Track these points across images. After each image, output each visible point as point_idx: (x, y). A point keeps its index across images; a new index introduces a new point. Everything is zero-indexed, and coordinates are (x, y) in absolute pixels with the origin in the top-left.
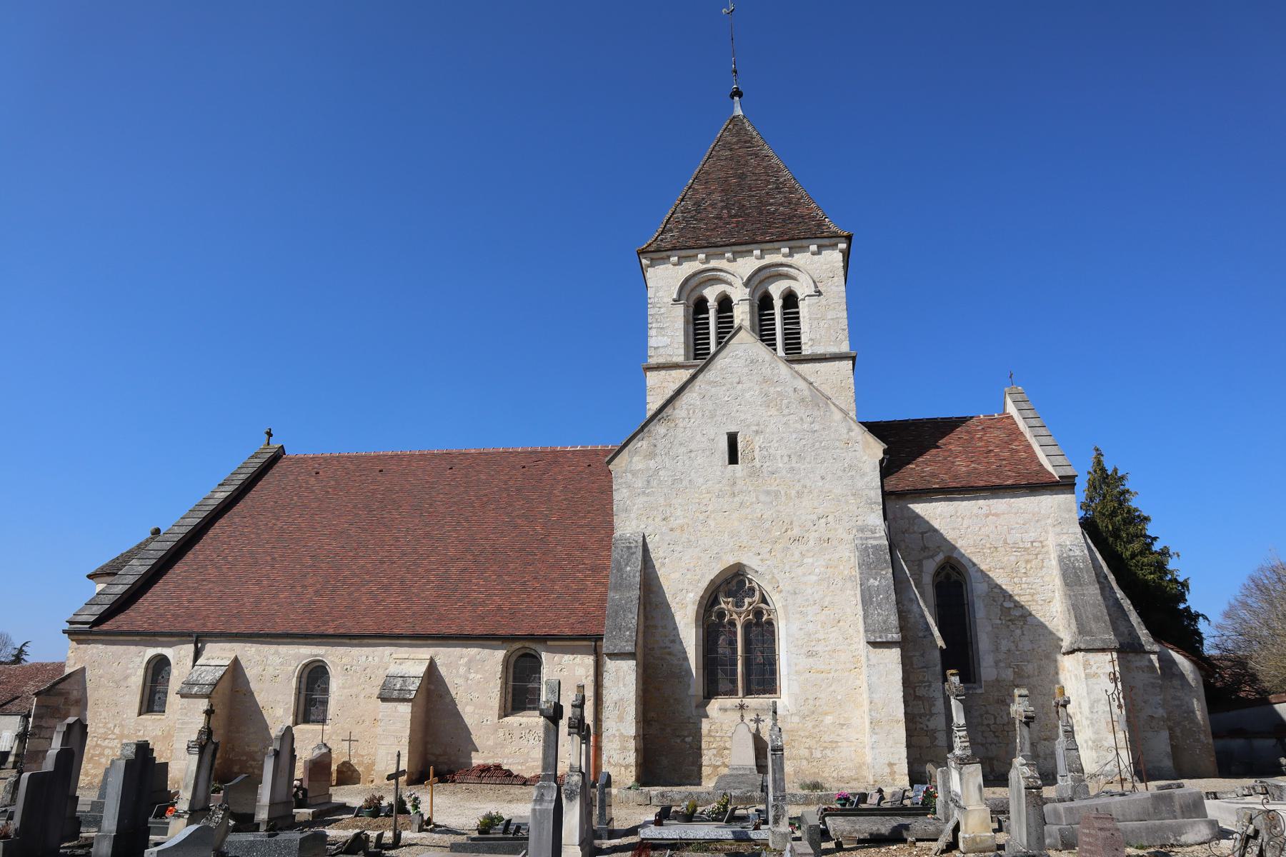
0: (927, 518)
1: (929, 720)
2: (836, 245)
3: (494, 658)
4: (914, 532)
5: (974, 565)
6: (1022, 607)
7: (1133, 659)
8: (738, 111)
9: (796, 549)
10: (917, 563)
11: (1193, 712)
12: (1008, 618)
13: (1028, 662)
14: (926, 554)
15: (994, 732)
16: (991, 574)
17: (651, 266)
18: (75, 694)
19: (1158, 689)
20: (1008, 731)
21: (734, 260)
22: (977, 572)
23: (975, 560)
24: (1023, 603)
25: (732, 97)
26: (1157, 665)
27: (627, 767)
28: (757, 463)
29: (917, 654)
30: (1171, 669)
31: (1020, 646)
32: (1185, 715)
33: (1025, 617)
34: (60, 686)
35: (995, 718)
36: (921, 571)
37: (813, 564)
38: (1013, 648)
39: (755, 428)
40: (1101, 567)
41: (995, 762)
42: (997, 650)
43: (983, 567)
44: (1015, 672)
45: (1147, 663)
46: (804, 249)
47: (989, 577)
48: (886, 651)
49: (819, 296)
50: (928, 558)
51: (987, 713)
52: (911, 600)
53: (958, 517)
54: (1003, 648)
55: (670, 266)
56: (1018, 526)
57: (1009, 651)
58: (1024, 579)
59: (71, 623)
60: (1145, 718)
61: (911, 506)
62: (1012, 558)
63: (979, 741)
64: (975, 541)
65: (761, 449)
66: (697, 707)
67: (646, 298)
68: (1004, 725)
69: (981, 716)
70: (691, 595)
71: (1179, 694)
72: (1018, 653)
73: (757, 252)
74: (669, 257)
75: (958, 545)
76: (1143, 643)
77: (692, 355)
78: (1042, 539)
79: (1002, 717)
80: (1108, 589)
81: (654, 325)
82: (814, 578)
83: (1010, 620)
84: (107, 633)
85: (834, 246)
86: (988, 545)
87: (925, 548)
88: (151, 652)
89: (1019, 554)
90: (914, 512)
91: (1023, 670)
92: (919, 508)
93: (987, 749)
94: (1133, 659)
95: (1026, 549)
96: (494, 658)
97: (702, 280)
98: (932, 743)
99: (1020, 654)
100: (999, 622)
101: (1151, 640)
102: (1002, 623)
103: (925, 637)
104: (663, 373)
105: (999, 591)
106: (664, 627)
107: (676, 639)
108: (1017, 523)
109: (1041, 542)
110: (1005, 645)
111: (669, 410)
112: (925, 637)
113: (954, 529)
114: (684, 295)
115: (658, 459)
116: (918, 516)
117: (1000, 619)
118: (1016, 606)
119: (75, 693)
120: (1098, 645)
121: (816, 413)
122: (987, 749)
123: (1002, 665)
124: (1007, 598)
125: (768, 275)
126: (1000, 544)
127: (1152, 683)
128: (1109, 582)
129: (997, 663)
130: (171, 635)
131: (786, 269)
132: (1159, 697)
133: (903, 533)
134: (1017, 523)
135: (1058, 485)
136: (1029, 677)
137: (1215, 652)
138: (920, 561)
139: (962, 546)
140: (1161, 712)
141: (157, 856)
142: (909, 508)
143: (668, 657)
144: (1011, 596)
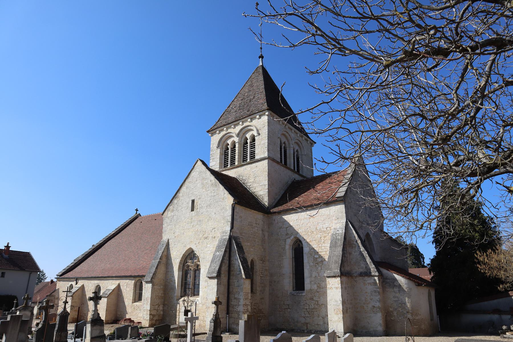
0: (288, 221)
1: (238, 307)
3: (131, 283)
4: (284, 228)
5: (304, 240)
6: (322, 257)
7: (367, 279)
9: (206, 241)
10: (284, 240)
11: (405, 304)
12: (316, 262)
13: (323, 281)
14: (287, 237)
15: (309, 312)
16: (311, 243)
17: (212, 136)
18: (57, 296)
19: (378, 293)
20: (314, 312)
21: (235, 128)
22: (305, 243)
23: (305, 238)
24: (322, 255)
26: (378, 282)
27: (147, 320)
29: (236, 281)
30: (394, 283)
31: (320, 274)
32: (400, 305)
33: (323, 262)
34: (53, 294)
35: (309, 306)
36: (285, 244)
37: (209, 247)
38: (317, 275)
39: (199, 197)
40: (355, 237)
41: (308, 325)
42: (311, 276)
43: (308, 241)
44: (317, 286)
45: (373, 281)
46: (255, 118)
47: (310, 245)
48: (213, 280)
49: (259, 135)
50: (288, 238)
51: (306, 304)
52: (236, 259)
53: (299, 220)
54: (314, 276)
55: (217, 135)
56: (321, 221)
57: (316, 277)
58: (323, 245)
59: (57, 275)
60: (371, 307)
61: (283, 217)
62: (319, 236)
63: (303, 316)
64: (305, 229)
66: (176, 300)
67: (210, 148)
68: (312, 309)
69: (304, 305)
70: (178, 260)
71: (397, 295)
72: (319, 277)
75: (299, 232)
76: (372, 272)
77: (223, 167)
78: (330, 226)
79: (311, 306)
80: (357, 247)
81: (212, 158)
82: (209, 252)
83: (316, 263)
84: (64, 278)
86: (310, 231)
87: (287, 234)
89: (321, 234)
90: (284, 219)
91: (320, 285)
92: (287, 217)
93: (305, 319)
94: (367, 279)
95: (324, 231)
96: (131, 283)
97: (226, 138)
98: (238, 317)
99: (320, 278)
100: (312, 264)
101: (376, 270)
102: (313, 265)
103: (239, 274)
105: (313, 250)
106: (171, 272)
107: (173, 277)
108: (321, 220)
109: (330, 228)
110: (314, 274)
111: (178, 194)
112: (239, 274)
113: (298, 225)
114: (221, 144)
115: (174, 212)
116: (285, 221)
117: (313, 263)
118: (319, 257)
119: (57, 296)
120: (332, 275)
121: (215, 189)
122: (305, 319)
123: (313, 283)
124: (316, 254)
125: (245, 131)
126: (314, 230)
127: (375, 291)
128: (358, 244)
129: (311, 282)
130: (116, 277)
131: (250, 127)
132: (378, 297)
133: (280, 228)
134: (321, 220)
135: (337, 201)
136: (323, 288)
137: (432, 273)
138: (285, 240)
139: (300, 232)
140: (378, 304)
141: (91, 341)
142: (283, 218)
143: (171, 282)
144: (317, 253)
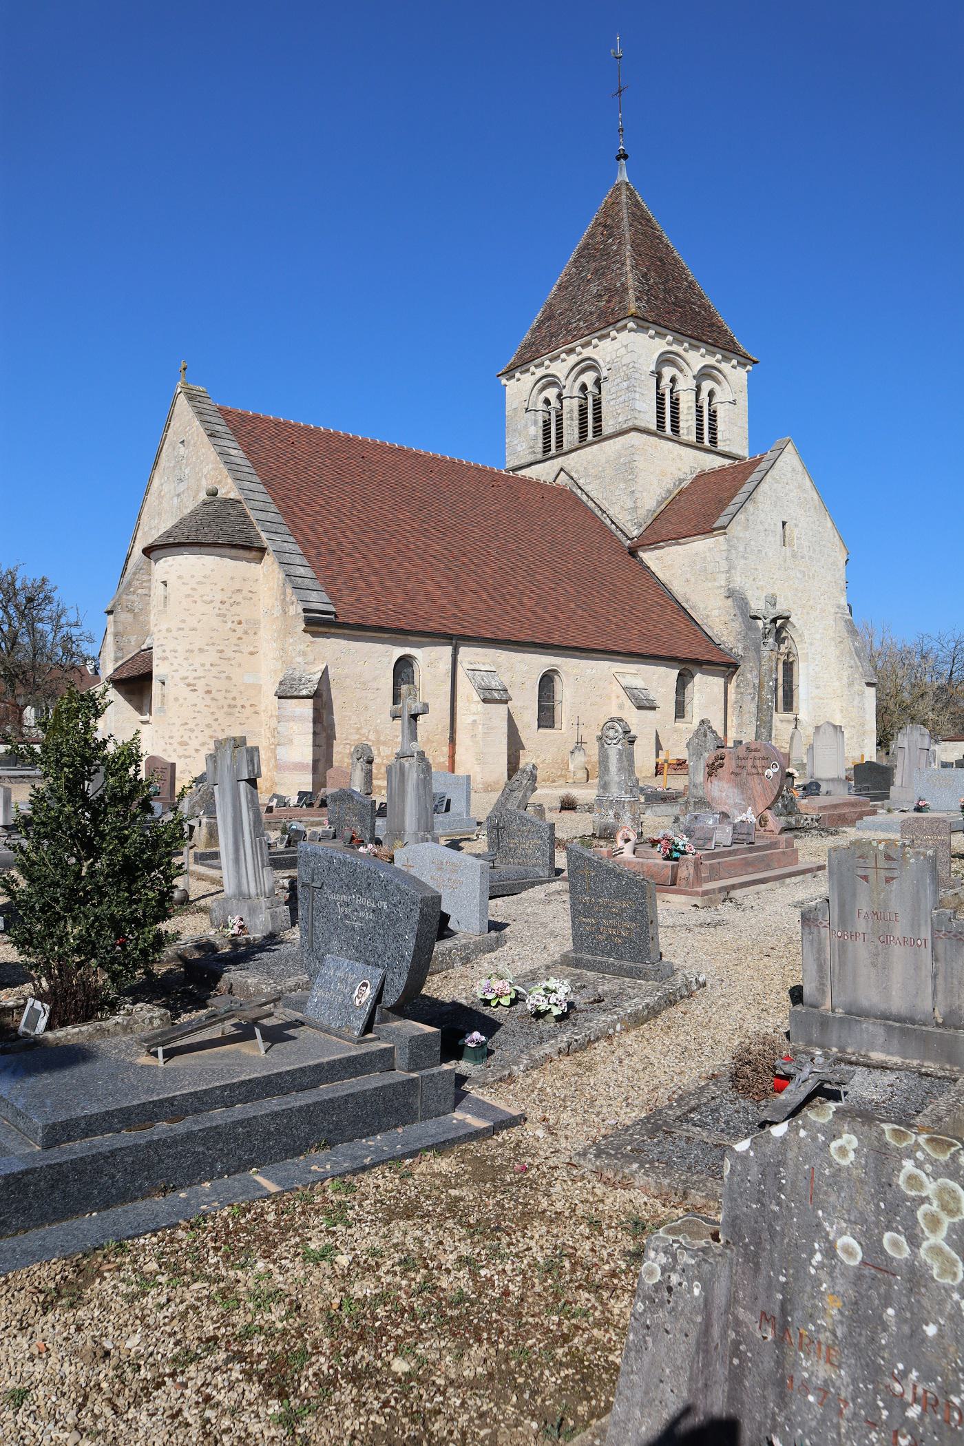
2: (666, 335)
8: (623, 176)
25: (618, 159)
28: (795, 548)
46: (697, 348)
65: (798, 538)
73: (670, 338)
74: (648, 328)
85: (744, 365)
88: (399, 652)
104: (644, 436)
